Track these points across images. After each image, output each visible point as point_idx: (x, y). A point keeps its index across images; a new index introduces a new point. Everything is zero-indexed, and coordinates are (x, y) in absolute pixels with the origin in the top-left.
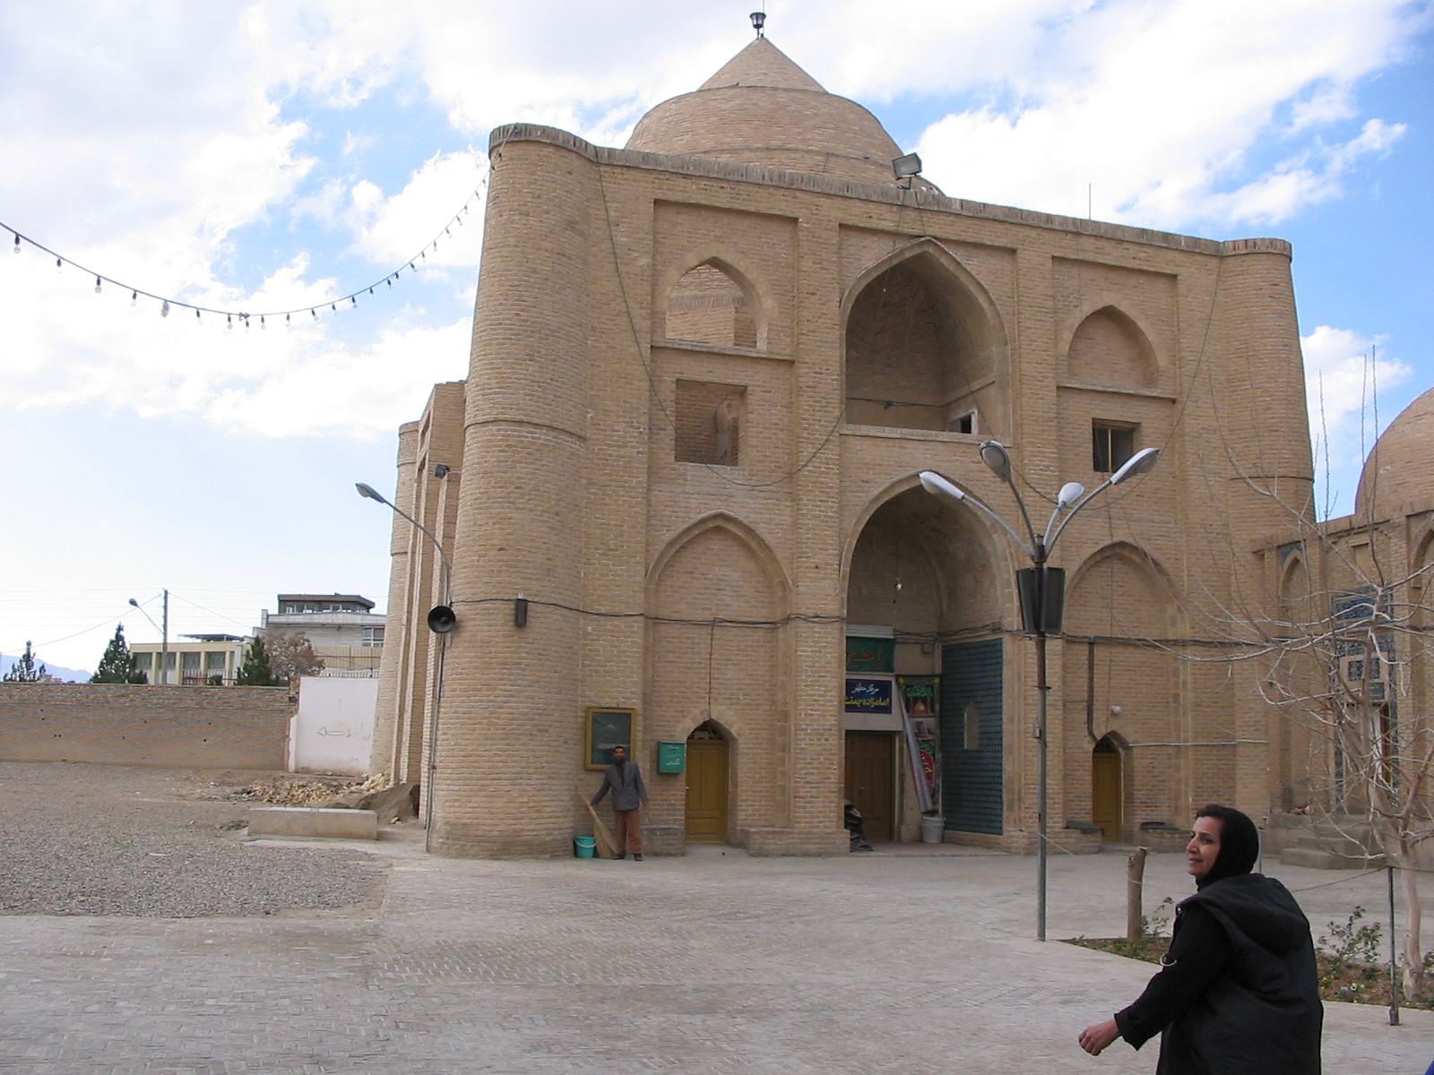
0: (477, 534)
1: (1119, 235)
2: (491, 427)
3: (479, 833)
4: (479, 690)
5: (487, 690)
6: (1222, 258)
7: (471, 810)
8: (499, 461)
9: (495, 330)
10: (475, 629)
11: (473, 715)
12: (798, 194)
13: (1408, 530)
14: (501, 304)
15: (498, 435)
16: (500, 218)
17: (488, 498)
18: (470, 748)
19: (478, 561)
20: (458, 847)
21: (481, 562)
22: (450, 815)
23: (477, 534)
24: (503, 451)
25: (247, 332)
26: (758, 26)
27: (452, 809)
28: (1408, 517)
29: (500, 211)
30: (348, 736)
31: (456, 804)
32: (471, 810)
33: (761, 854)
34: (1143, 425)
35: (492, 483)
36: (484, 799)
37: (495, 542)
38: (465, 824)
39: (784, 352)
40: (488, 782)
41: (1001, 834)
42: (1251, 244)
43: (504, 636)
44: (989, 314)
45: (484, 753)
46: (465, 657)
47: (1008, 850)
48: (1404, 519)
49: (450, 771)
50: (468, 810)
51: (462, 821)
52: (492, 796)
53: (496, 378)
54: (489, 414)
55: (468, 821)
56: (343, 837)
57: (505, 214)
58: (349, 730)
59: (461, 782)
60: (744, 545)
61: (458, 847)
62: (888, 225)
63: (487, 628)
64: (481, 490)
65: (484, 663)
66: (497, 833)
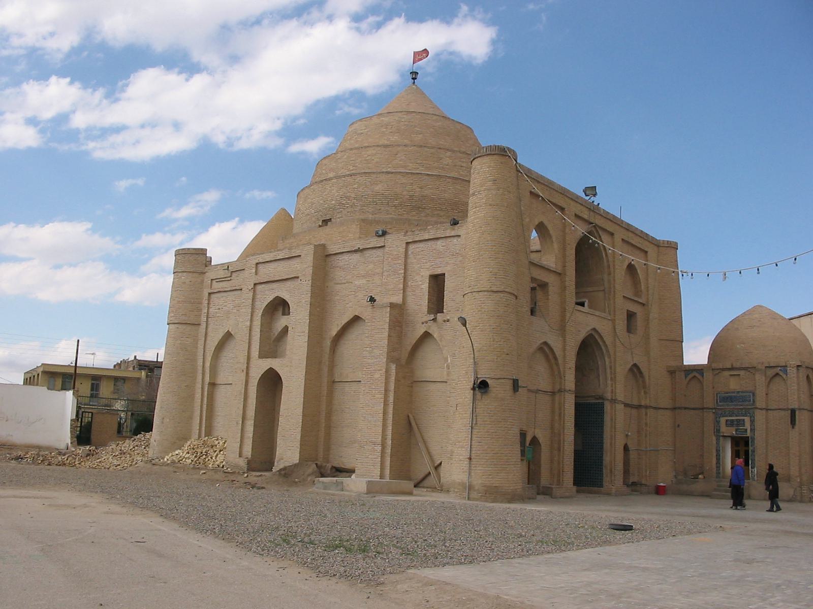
0: (496, 346)
1: (637, 232)
2: (500, 294)
3: (504, 491)
4: (501, 422)
5: (504, 422)
6: (658, 246)
7: (499, 480)
8: (505, 311)
9: (501, 247)
10: (497, 392)
11: (498, 434)
12: (566, 198)
13: (765, 372)
14: (503, 235)
15: (504, 298)
16: (498, 192)
17: (501, 329)
18: (497, 449)
19: (497, 359)
20: (492, 497)
21: (499, 360)
22: (486, 482)
23: (496, 346)
24: (506, 307)
25: (692, 278)
26: (414, 79)
27: (487, 479)
28: (766, 367)
29: (498, 188)
30: (7, 421)
31: (490, 477)
32: (499, 480)
33: (556, 498)
34: (638, 314)
35: (502, 322)
36: (504, 474)
37: (505, 350)
38: (496, 486)
39: (559, 270)
40: (507, 466)
41: (602, 487)
42: (669, 243)
43: (510, 396)
44: (605, 261)
45: (504, 452)
46: (492, 405)
47: (609, 494)
48: (764, 368)
49: (484, 461)
50: (497, 480)
51: (494, 485)
52: (508, 473)
53: (503, 271)
54: (499, 288)
55: (497, 485)
56: (397, 494)
57: (501, 190)
58: (7, 417)
59: (492, 466)
60: (547, 357)
61: (492, 497)
62: (586, 217)
63: (503, 392)
64: (497, 324)
65: (502, 409)
66: (510, 491)
